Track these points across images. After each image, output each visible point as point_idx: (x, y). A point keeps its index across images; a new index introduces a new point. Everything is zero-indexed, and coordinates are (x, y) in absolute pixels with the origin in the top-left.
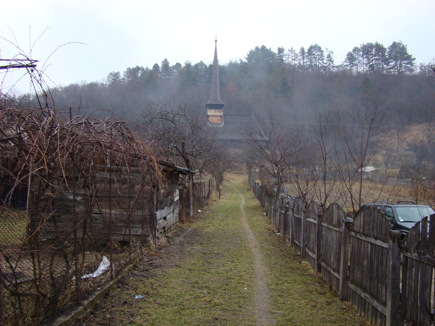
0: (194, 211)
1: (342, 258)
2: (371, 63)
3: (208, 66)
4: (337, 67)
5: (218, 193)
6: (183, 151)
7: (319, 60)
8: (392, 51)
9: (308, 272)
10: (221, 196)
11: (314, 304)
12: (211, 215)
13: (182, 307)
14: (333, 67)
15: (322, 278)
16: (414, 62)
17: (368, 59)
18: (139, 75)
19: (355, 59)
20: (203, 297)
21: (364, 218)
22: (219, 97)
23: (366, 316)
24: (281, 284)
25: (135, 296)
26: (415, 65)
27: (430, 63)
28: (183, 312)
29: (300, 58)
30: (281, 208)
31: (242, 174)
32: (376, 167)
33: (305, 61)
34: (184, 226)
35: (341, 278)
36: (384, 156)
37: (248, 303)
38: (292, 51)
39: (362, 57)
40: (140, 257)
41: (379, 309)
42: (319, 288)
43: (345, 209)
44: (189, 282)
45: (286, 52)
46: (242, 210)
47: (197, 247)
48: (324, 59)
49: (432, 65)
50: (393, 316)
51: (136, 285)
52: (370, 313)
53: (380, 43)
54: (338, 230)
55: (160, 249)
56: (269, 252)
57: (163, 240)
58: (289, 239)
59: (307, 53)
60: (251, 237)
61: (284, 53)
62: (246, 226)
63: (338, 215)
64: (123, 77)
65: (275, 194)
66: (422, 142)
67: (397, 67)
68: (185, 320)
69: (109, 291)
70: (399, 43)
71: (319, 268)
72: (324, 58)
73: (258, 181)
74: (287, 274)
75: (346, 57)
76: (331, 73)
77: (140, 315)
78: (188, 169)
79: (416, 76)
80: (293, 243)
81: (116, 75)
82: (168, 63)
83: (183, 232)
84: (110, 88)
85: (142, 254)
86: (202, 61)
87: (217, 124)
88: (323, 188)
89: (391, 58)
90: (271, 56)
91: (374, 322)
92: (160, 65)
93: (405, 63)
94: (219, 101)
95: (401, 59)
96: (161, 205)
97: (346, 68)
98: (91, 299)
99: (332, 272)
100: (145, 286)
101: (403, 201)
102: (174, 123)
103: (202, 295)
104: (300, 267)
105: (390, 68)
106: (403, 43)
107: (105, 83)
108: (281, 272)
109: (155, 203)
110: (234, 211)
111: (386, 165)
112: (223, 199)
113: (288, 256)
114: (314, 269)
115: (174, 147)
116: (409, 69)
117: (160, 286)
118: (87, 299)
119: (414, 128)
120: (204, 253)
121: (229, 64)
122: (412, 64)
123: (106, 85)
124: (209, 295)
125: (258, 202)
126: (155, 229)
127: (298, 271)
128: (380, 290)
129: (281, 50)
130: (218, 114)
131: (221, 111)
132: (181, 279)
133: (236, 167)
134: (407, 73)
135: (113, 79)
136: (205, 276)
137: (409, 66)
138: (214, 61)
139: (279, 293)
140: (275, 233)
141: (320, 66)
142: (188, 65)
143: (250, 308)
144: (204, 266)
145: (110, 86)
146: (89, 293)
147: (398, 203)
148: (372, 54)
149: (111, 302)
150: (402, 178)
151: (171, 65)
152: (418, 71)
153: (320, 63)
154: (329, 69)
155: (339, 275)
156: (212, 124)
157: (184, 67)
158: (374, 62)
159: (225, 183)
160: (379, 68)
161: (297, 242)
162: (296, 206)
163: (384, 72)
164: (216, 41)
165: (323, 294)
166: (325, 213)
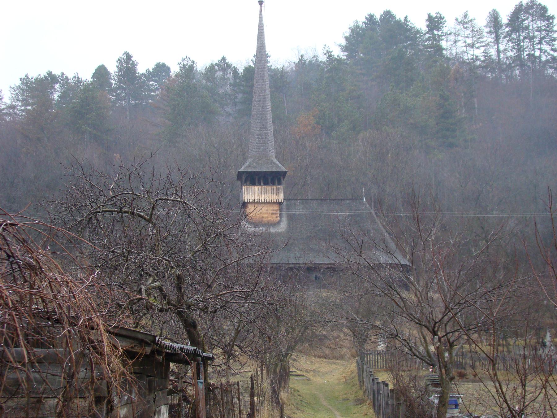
3: (241, 70)
6: (180, 302)
7: (540, 43)
18: (56, 96)
29: (489, 39)
31: (341, 357)
38: (465, 21)
45: (449, 25)
59: (507, 25)
65: (434, 412)
73: (383, 377)
78: (193, 348)
82: (134, 65)
86: (224, 59)
87: (270, 225)
90: (408, 38)
92: (113, 69)
102: (154, 225)
115: (154, 288)
129: (435, 23)
133: (321, 339)
138: (256, 56)
141: (544, 58)
151: (141, 69)
156: (255, 225)
157: (177, 75)
159: (293, 383)
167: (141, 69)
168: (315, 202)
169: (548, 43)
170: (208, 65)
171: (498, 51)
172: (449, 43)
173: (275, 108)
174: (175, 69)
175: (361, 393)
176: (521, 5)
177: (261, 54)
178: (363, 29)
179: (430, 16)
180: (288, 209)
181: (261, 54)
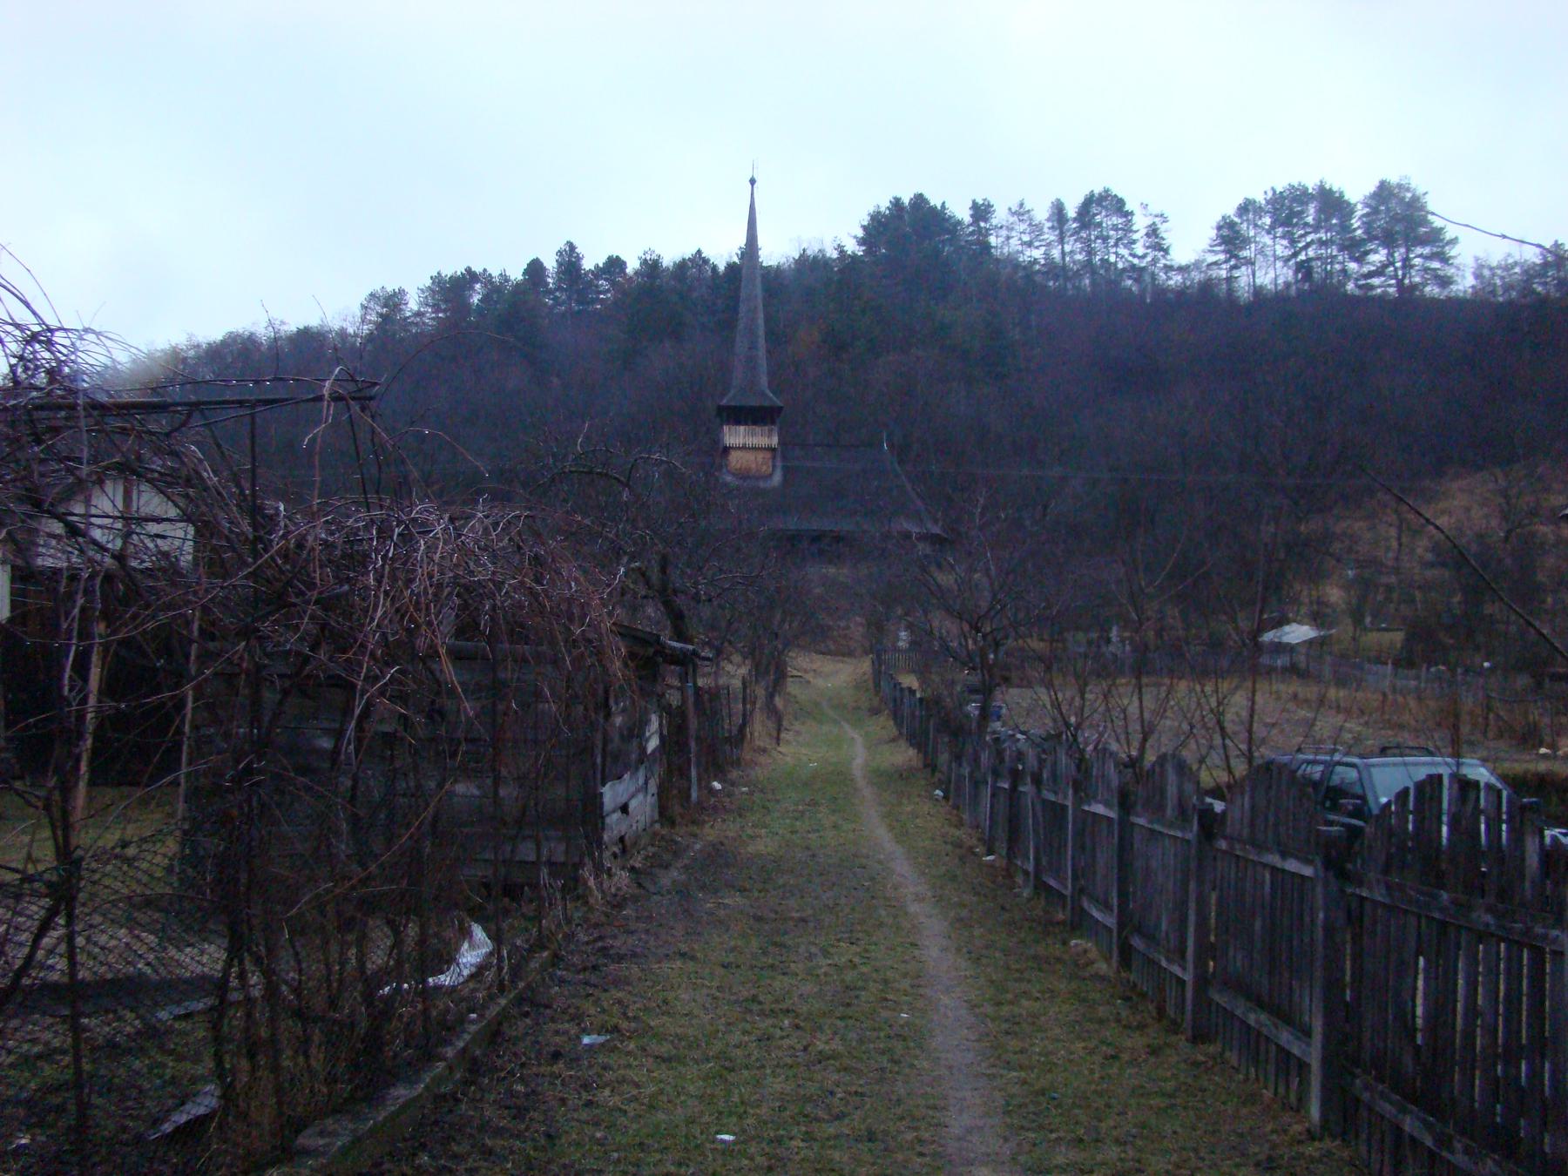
0: (700, 788)
1: (1192, 918)
2: (1302, 257)
3: (722, 268)
4: (1182, 269)
5: (771, 725)
7: (1116, 245)
8: (1375, 211)
9: (1091, 970)
10: (783, 735)
11: (1111, 1051)
12: (757, 796)
13: (727, 1064)
14: (1168, 268)
15: (1135, 985)
16: (1452, 253)
17: (1293, 242)
18: (475, 299)
19: (1246, 241)
20: (782, 1038)
21: (1252, 798)
22: (764, 380)
23: (1261, 1077)
24: (1011, 1003)
25: (579, 1038)
26: (1456, 262)
27: (1509, 255)
28: (731, 1077)
29: (1051, 236)
30: (996, 774)
31: (850, 654)
32: (1318, 626)
33: (1067, 248)
34: (680, 835)
35: (1188, 977)
36: (1347, 586)
37: (918, 1052)
38: (1020, 212)
39: (1268, 233)
40: (566, 929)
41: (1295, 1051)
42: (1124, 1014)
43: (1206, 779)
44: (733, 998)
45: (1000, 216)
46: (861, 783)
47: (733, 900)
48: (1134, 242)
49: (1516, 263)
50: (1326, 1061)
51: (577, 1008)
52: (1271, 1068)
53: (1335, 183)
54: (1179, 834)
55: (619, 906)
56: (964, 913)
57: (622, 878)
58: (1026, 873)
59: (1075, 220)
60: (902, 868)
61: (994, 222)
62: (882, 834)
63: (1181, 791)
64: (415, 308)
65: (974, 726)
66: (1480, 537)
67: (1396, 269)
68: (741, 1095)
69: (500, 1024)
70: (1400, 186)
71: (1126, 955)
72: (1135, 237)
73: (909, 681)
74: (1026, 975)
75: (1213, 233)
76: (1160, 292)
77: (607, 1085)
79: (1456, 304)
80: (1041, 887)
81: (393, 301)
82: (579, 258)
83: (676, 855)
84: (369, 347)
85: (569, 921)
86: (699, 252)
88: (1136, 703)
89: (1372, 238)
90: (948, 231)
91: (1281, 1090)
92: (550, 263)
93: (1420, 256)
94: (763, 394)
95: (1407, 239)
96: (615, 768)
97: (1214, 273)
98: (461, 1044)
99: (1164, 964)
100: (604, 1011)
101: (1411, 744)
102: (631, 490)
103: (779, 1033)
104: (1066, 957)
105: (1371, 275)
106: (1413, 186)
107: (351, 331)
108: (1008, 968)
109: (599, 760)
110: (831, 787)
111: (1358, 620)
112: (788, 742)
113: (1026, 924)
114: (1108, 960)
116: (1437, 277)
117: (646, 1009)
118: (447, 1042)
119: (1455, 486)
120: (759, 919)
121: (797, 262)
122: (1445, 260)
123: (356, 335)
124: (799, 1033)
125: (912, 752)
126: (600, 842)
127: (1058, 966)
128: (1296, 998)
129: (981, 211)
130: (763, 441)
131: (770, 431)
132: (705, 991)
134: (1432, 290)
135: (381, 315)
136: (777, 984)
137: (1435, 265)
139: (1005, 1026)
140: (975, 854)
141: (1120, 266)
142: (651, 267)
143: (925, 1064)
144: (765, 953)
145: (370, 338)
146: (451, 1027)
147: (1384, 751)
148: (1306, 224)
149: (515, 1054)
150: (1411, 664)
151: (588, 264)
152: (1465, 283)
153: (1119, 257)
154: (1153, 276)
155: (1184, 969)
157: (636, 273)
158: (1311, 253)
159: (792, 687)
160: (1329, 274)
161: (1052, 883)
162: (1048, 764)
163: (1350, 286)
164: (753, 182)
165: (1138, 1027)
166: (1139, 786)
167: (588, 264)
168: (819, 449)
169: (1125, 246)
170: (678, 259)
171: (1063, 254)
172: (1000, 240)
173: (767, 319)
174: (632, 265)
175: (876, 702)
176: (1092, 194)
177: (751, 248)
178: (884, 216)
179: (974, 203)
180: (784, 458)
181: (751, 248)
